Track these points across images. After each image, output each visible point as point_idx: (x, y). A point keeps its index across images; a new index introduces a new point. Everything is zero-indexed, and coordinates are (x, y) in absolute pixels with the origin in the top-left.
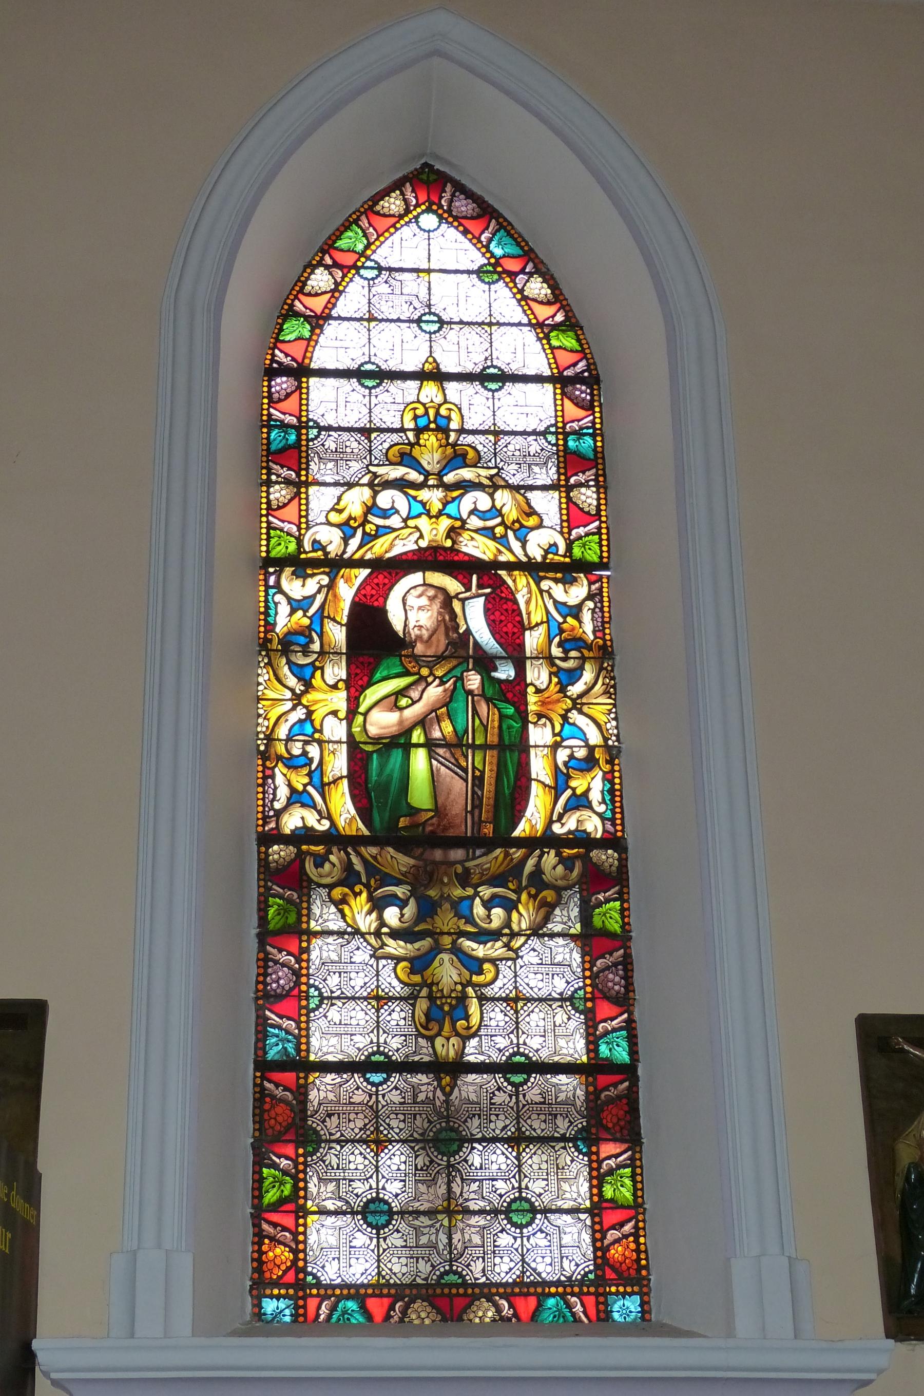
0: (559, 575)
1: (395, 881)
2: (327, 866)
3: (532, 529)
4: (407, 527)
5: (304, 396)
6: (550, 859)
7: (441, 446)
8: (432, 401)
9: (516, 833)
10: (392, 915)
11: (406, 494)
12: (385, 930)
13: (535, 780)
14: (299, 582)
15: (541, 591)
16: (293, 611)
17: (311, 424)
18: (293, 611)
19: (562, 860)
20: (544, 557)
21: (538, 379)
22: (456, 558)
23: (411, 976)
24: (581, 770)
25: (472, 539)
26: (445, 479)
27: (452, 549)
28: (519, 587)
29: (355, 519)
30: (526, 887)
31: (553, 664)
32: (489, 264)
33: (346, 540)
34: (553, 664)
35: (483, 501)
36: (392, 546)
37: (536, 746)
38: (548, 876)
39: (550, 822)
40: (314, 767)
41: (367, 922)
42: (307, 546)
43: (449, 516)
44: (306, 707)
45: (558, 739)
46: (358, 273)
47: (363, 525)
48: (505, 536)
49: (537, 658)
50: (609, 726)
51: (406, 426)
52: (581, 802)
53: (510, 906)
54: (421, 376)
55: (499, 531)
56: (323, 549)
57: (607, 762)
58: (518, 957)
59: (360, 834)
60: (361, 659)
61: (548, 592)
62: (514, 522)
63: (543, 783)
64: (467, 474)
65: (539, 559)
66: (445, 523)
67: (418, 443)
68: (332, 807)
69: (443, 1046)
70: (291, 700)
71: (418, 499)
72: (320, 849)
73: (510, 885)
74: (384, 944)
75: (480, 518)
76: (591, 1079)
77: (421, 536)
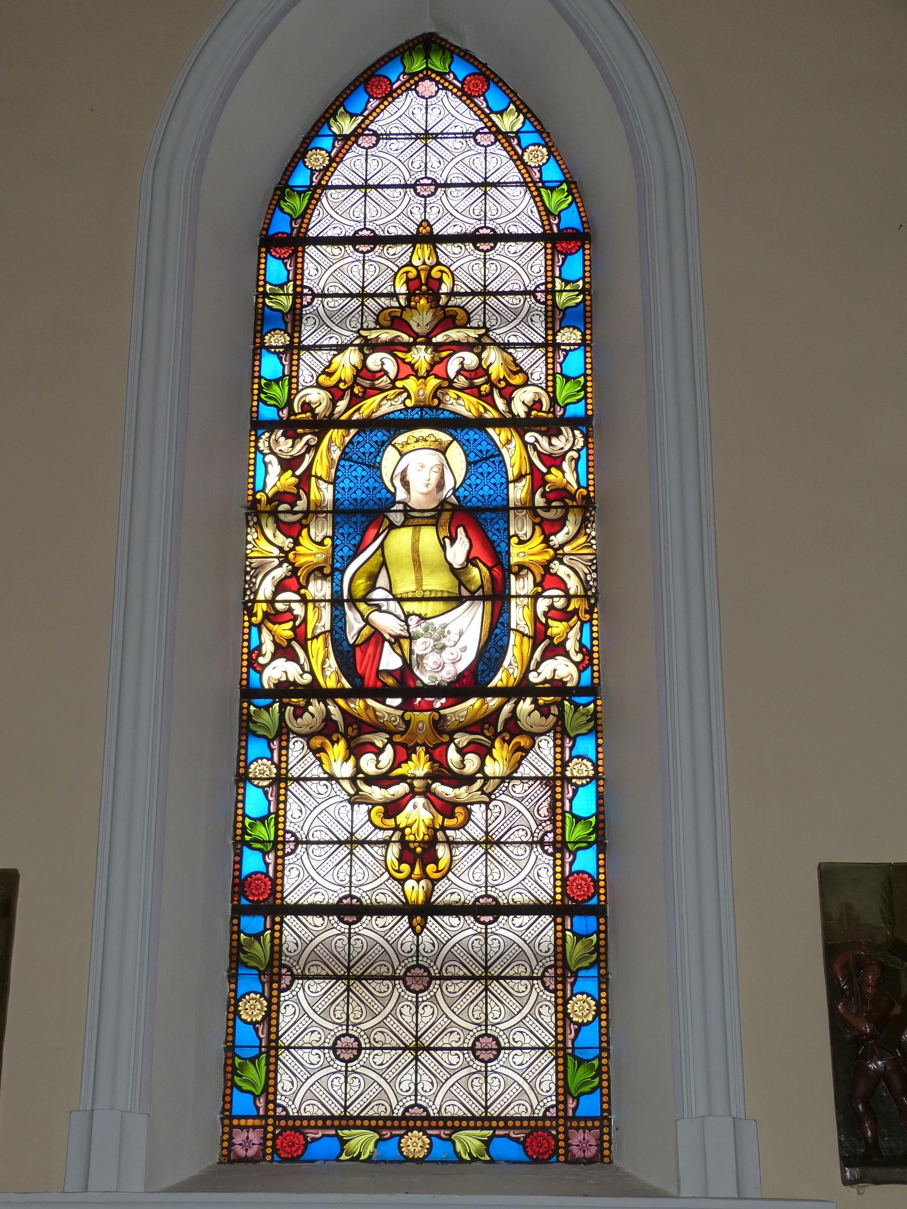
0: (543, 429)
1: (373, 729)
2: (306, 715)
3: (518, 387)
4: (394, 387)
6: (526, 705)
7: (431, 308)
10: (368, 763)
11: (396, 357)
12: (361, 776)
14: (560, 674)
15: (312, 672)
16: (284, 470)
17: (306, 291)
19: (538, 707)
20: (528, 414)
21: (299, 910)
22: (442, 416)
25: (459, 397)
28: (333, 677)
29: (345, 383)
31: (536, 515)
32: (486, 127)
33: (334, 402)
34: (536, 515)
35: (470, 360)
36: (379, 406)
37: (518, 596)
38: (524, 724)
40: (297, 623)
42: (297, 408)
43: (437, 377)
44: (549, 546)
45: (540, 589)
46: (356, 142)
48: (491, 394)
49: (522, 508)
50: (255, 536)
51: (398, 291)
52: (287, 464)
53: (484, 752)
54: (414, 240)
55: (485, 388)
56: (312, 410)
58: (358, 332)
60: (353, 519)
65: (523, 415)
66: (433, 382)
69: (413, 888)
71: (407, 360)
72: (302, 702)
73: (486, 732)
74: (359, 790)
76: (559, 920)
77: (409, 397)
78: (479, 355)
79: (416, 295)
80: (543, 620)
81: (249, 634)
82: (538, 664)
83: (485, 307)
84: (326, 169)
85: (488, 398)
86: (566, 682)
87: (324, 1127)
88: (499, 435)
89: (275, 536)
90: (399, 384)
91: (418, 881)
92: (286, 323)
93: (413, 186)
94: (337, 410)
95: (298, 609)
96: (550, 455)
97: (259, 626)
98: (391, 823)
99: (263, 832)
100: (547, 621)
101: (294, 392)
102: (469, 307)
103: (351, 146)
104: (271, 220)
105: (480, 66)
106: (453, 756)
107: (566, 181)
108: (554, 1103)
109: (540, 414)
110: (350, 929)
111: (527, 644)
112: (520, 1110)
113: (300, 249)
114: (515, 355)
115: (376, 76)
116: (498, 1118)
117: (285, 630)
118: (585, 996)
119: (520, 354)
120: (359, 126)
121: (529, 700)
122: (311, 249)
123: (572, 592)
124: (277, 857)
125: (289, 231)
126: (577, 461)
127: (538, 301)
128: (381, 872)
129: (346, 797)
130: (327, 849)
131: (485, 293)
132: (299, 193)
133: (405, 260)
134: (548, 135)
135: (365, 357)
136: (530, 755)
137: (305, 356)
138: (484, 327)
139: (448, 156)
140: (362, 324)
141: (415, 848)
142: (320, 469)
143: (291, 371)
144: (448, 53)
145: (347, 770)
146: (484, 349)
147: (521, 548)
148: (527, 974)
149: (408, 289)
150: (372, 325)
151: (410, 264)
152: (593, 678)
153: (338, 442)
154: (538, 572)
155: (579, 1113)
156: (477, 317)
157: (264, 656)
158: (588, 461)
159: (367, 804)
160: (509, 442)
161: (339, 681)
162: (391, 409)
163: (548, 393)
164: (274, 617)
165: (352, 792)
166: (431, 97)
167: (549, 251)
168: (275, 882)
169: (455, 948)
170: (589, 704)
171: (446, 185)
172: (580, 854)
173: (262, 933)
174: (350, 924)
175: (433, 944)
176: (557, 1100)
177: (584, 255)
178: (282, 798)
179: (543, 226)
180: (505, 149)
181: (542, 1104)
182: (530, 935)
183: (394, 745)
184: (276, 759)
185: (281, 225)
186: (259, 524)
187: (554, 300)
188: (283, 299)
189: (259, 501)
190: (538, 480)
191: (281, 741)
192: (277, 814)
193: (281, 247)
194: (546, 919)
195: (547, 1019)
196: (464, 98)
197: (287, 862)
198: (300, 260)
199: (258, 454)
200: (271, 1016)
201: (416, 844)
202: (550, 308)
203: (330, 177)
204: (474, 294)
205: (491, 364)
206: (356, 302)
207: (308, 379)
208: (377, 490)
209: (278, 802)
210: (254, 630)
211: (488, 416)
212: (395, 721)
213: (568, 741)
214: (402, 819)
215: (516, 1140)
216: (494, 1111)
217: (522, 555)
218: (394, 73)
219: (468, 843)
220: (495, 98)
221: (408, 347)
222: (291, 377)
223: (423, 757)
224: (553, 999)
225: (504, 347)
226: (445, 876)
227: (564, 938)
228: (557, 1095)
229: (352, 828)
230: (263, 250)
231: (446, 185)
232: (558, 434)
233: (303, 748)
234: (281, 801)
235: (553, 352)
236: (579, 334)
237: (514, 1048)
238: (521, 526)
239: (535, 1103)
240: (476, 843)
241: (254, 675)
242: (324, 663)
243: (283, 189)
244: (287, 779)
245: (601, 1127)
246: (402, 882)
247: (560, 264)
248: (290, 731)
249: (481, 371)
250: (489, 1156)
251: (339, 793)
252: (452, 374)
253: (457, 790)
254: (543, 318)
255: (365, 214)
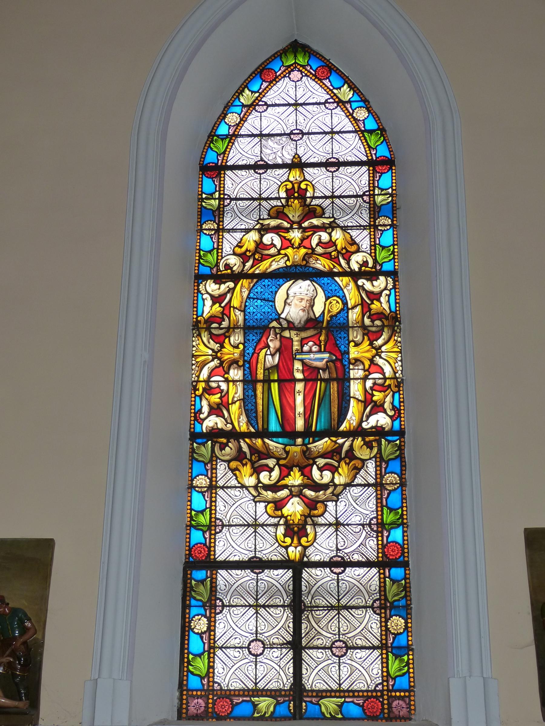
0: (368, 277)
2: (227, 449)
5: (222, 182)
6: (358, 442)
7: (301, 206)
8: (296, 180)
9: (342, 428)
10: (264, 477)
11: (280, 236)
12: (260, 485)
13: (352, 397)
15: (232, 423)
16: (214, 303)
17: (226, 197)
18: (214, 303)
20: (360, 269)
23: (275, 512)
24: (215, 316)
25: (318, 259)
26: (303, 225)
27: (305, 266)
29: (250, 251)
30: (344, 458)
33: (244, 264)
35: (325, 237)
36: (270, 265)
38: (357, 453)
39: (361, 421)
40: (223, 394)
41: (251, 481)
42: (222, 268)
43: (305, 248)
47: (254, 254)
48: (338, 257)
51: (281, 196)
52: (216, 299)
53: (334, 470)
56: (231, 268)
57: (396, 386)
58: (257, 221)
59: (341, 278)
61: (362, 286)
62: (342, 249)
63: (357, 399)
64: (315, 222)
65: (357, 270)
66: (303, 251)
67: (288, 205)
68: (357, 293)
70: (382, 352)
72: (224, 440)
73: (335, 458)
74: (259, 493)
75: (323, 248)
77: (288, 260)
78: (330, 234)
79: (291, 198)
80: (370, 392)
81: (195, 401)
82: (368, 417)
83: (333, 205)
84: (238, 125)
85: (336, 260)
86: (385, 428)
87: (244, 696)
88: (342, 281)
89: (209, 343)
90: (283, 252)
91: (296, 548)
92: (215, 217)
93: (289, 135)
94: (246, 268)
95: (224, 386)
96: (372, 293)
97: (200, 397)
98: (279, 513)
99: (203, 520)
100: (372, 392)
101: (220, 258)
102: (324, 205)
103: (252, 111)
104: (389, 148)
105: (325, 61)
106: (316, 473)
107: (378, 129)
108: (381, 681)
109: (367, 269)
110: (257, 577)
111: (361, 406)
112: (360, 686)
113: (222, 172)
114: (351, 234)
115: (266, 69)
116: (348, 691)
117: (215, 399)
118: (200, 616)
119: (354, 233)
120: (257, 99)
121: (360, 439)
122: (229, 173)
123: (387, 375)
124: (211, 534)
125: (216, 161)
126: (389, 296)
127: (365, 201)
128: (273, 543)
129: (252, 498)
130: (241, 529)
131: (333, 197)
132: (222, 139)
133: (285, 178)
134: (369, 102)
135: (262, 236)
136: (361, 472)
137: (226, 235)
138: (333, 217)
139: (310, 116)
140: (260, 216)
141: (294, 528)
142: (236, 303)
143: (218, 245)
144: (307, 54)
145: (251, 481)
146: (333, 230)
147: (356, 349)
148: (281, 604)
149: (287, 195)
150: (266, 217)
151: (288, 180)
152: (401, 425)
153: (247, 286)
154: (367, 363)
155: (395, 688)
156: (328, 211)
157: (203, 414)
158: (396, 296)
159: (264, 502)
160: (347, 285)
161: (248, 429)
162: (278, 267)
163: (372, 256)
164: (209, 390)
165: (255, 494)
166: (298, 81)
167: (371, 172)
168: (209, 548)
169: (320, 589)
170: (397, 440)
171: (309, 134)
172: (392, 532)
173: (205, 580)
174: (257, 574)
175: (226, 586)
176: (382, 680)
177: (392, 173)
178: (214, 499)
179: (367, 156)
180: (344, 111)
181: (373, 682)
182: (364, 581)
183: (280, 466)
184: (209, 475)
185: (211, 158)
186: (199, 335)
187: (374, 200)
188: (212, 202)
189: (200, 322)
190: (365, 307)
191: (212, 465)
192: (210, 508)
193: (211, 171)
194: (374, 570)
195: (376, 631)
196: (316, 80)
197: (217, 537)
198: (222, 179)
199: (199, 294)
200: (211, 629)
201: (294, 526)
202: (372, 206)
203: (240, 130)
204: (326, 197)
205: (337, 239)
206: (256, 203)
207: (228, 249)
208: (270, 314)
209: (211, 502)
210: (198, 399)
211: (335, 270)
212: (279, 452)
213: (384, 464)
214: (286, 511)
215: (358, 705)
216: (345, 686)
217: (356, 353)
218: (276, 66)
219: (266, 525)
220: (336, 81)
221: (287, 230)
222: (218, 249)
223: (298, 474)
224: (379, 619)
225: (344, 229)
226: (312, 544)
227: (385, 582)
228: (383, 676)
229: (256, 516)
230: (201, 173)
231: (309, 134)
232: (377, 279)
233: (225, 469)
234: (213, 501)
235: (374, 232)
236: (390, 220)
237: (240, 648)
238: (356, 335)
239: (369, 682)
240: (330, 525)
241: (198, 426)
242: (239, 418)
243: (212, 136)
244: (216, 487)
245: (409, 696)
246: (286, 548)
247: (378, 178)
248: (217, 458)
249: (332, 243)
250: (342, 714)
251: (247, 495)
252: (314, 246)
253: (317, 494)
254: (368, 211)
255: (332, 149)
